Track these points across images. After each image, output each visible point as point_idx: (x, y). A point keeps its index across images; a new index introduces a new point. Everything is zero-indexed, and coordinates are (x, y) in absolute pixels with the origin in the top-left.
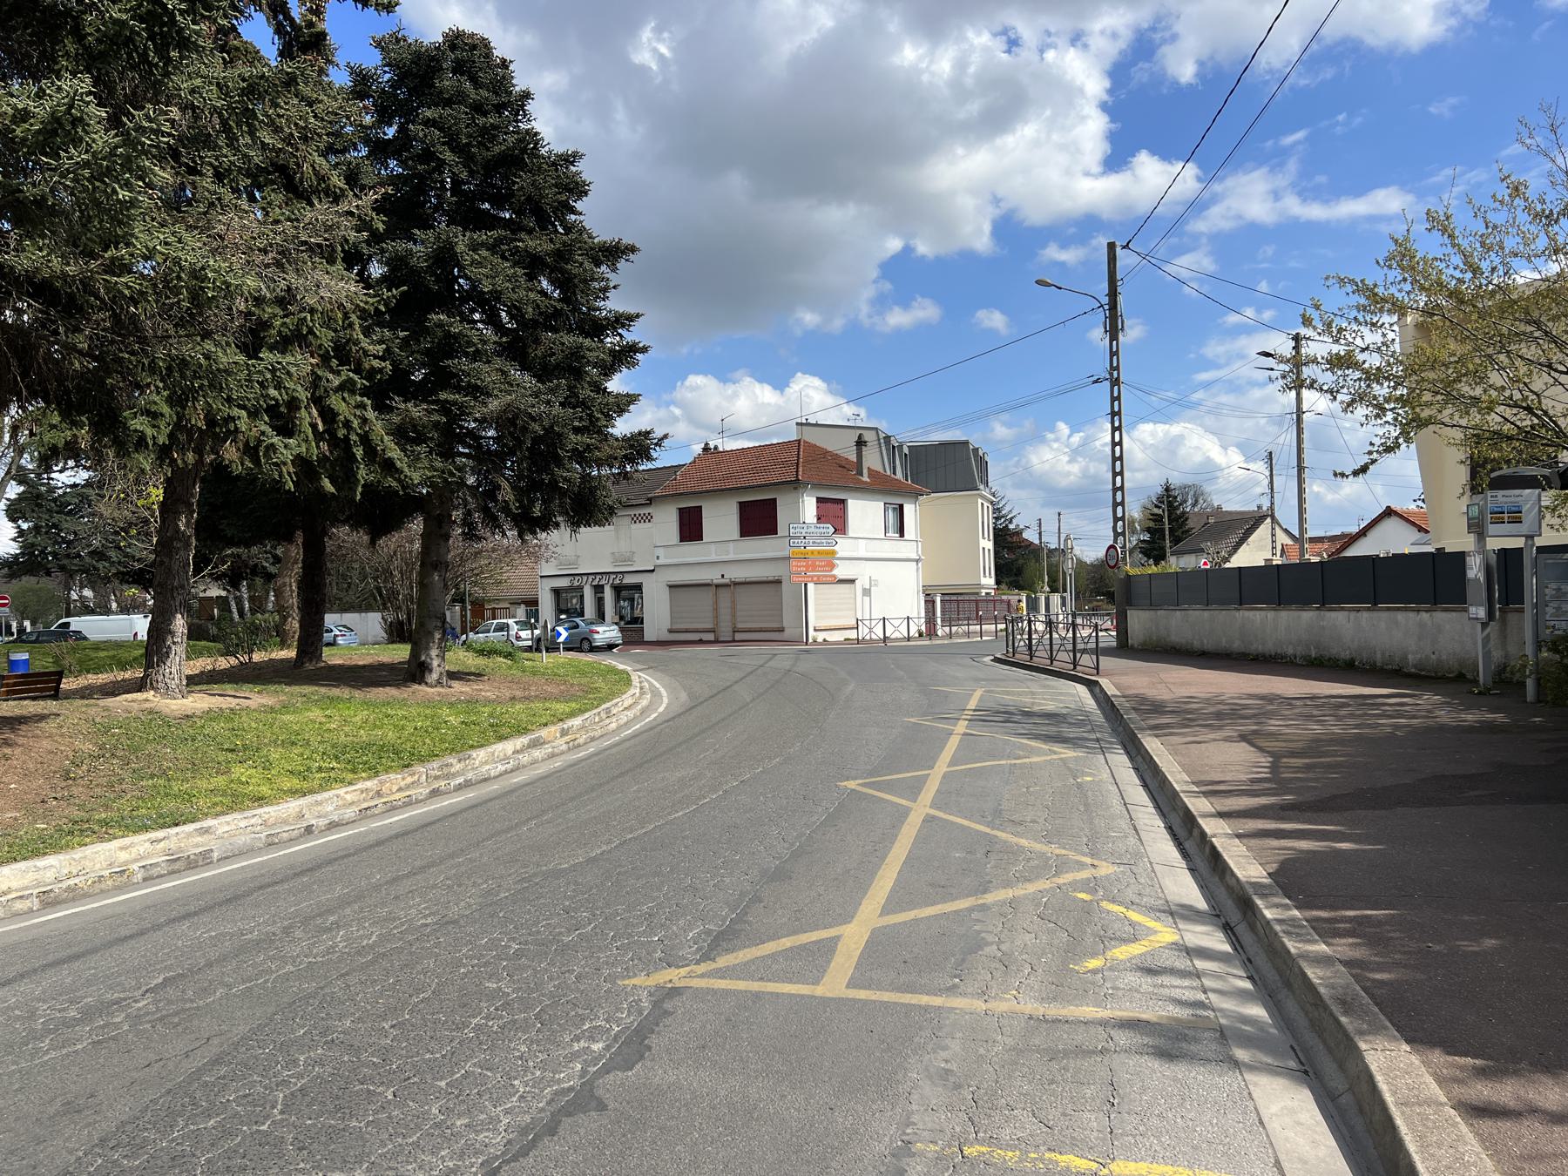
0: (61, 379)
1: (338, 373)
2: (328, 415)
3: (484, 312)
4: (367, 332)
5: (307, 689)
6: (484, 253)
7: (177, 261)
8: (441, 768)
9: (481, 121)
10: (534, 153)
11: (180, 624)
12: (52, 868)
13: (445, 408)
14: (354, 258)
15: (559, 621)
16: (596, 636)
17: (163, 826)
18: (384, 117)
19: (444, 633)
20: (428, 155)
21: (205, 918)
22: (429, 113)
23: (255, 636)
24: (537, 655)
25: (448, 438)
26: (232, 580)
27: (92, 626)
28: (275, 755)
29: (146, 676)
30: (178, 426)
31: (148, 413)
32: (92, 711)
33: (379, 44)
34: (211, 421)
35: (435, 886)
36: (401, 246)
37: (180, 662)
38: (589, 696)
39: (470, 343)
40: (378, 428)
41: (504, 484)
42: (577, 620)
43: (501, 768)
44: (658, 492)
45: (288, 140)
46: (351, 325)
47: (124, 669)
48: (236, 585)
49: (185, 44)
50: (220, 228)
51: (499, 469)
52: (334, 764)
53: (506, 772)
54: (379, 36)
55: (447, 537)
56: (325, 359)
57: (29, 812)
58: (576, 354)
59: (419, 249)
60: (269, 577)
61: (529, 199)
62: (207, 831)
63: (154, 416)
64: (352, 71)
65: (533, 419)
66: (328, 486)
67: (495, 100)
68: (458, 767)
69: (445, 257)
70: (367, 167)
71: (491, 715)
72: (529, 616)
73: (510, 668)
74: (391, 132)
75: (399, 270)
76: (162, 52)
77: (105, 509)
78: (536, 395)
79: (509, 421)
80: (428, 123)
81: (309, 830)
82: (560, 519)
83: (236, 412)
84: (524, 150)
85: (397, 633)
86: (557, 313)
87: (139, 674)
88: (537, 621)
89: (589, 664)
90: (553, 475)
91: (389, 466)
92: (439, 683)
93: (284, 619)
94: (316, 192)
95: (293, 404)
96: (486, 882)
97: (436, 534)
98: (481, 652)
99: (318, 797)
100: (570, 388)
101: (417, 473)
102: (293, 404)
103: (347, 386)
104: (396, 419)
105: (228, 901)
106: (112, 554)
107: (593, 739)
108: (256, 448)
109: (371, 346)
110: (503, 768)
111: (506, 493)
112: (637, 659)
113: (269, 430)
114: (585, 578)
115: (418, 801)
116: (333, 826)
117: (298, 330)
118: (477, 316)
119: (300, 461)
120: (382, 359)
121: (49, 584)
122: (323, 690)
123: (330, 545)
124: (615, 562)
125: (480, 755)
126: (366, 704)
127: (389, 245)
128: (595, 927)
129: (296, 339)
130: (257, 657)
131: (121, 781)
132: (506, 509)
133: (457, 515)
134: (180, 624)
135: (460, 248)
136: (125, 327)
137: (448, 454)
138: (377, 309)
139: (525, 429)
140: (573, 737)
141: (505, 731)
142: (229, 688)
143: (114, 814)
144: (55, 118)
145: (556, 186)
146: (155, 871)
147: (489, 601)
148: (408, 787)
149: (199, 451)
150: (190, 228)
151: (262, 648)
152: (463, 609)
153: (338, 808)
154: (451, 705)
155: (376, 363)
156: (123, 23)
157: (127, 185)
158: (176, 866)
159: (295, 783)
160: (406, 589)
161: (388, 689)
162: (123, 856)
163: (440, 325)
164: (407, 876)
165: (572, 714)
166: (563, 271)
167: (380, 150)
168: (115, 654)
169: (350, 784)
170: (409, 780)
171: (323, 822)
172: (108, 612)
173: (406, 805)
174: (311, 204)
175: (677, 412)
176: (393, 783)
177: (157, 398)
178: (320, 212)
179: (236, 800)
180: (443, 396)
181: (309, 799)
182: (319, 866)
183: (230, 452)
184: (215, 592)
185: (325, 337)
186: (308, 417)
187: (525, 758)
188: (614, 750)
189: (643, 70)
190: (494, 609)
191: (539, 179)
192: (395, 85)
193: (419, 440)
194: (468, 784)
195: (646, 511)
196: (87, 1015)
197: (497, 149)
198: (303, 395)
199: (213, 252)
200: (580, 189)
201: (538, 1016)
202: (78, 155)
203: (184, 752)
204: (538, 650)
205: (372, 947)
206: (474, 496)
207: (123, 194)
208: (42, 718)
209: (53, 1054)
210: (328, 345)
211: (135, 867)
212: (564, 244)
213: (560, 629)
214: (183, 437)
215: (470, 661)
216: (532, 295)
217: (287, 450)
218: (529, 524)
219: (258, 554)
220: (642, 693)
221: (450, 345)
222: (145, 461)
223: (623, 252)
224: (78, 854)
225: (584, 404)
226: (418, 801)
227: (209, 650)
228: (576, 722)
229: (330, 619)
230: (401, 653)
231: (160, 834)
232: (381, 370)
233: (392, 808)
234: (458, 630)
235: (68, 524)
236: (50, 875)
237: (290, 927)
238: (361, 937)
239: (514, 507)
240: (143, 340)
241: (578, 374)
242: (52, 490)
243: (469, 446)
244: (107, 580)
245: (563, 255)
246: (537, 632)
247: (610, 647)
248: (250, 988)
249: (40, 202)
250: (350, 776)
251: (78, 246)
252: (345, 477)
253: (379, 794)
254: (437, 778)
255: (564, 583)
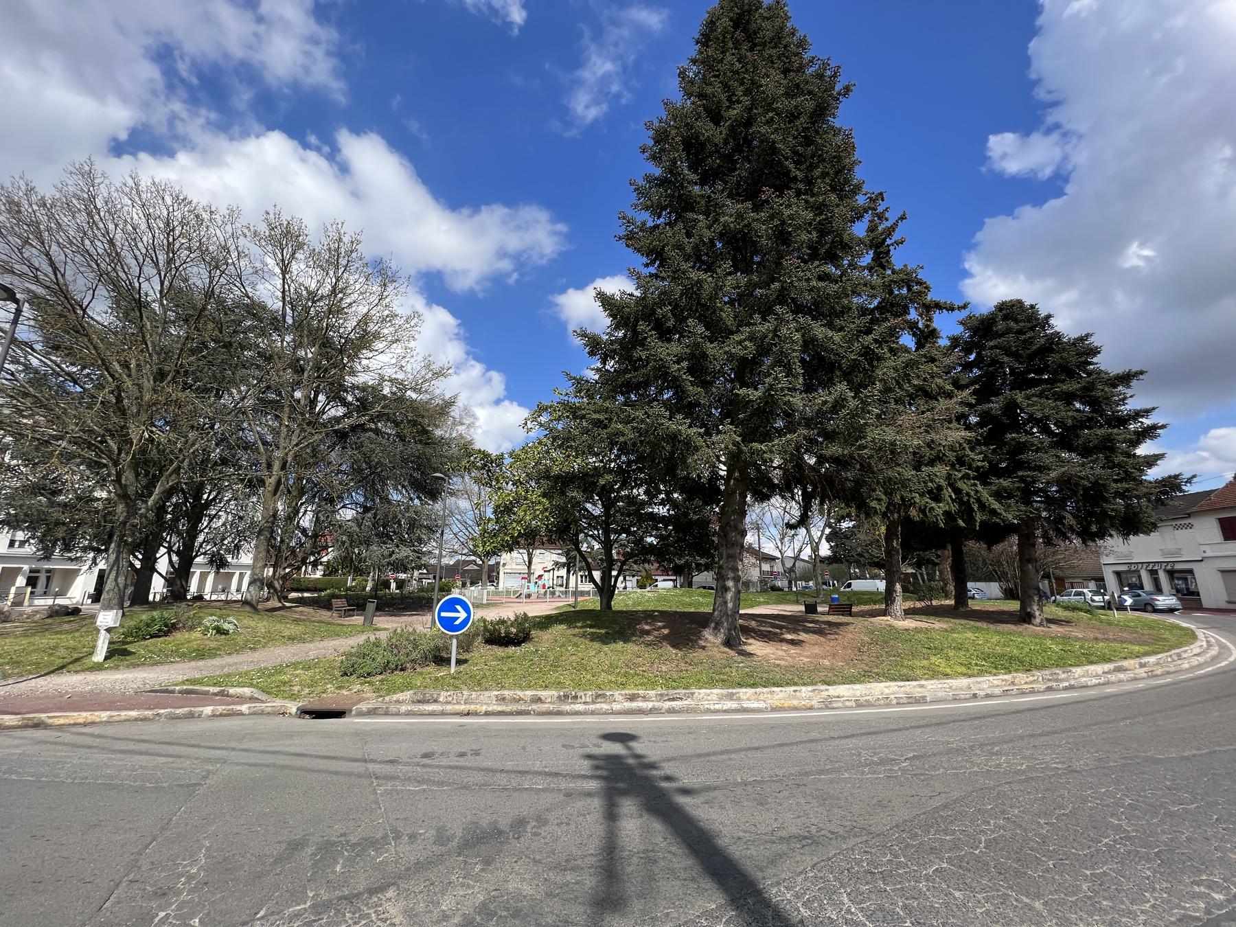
0: (844, 490)
1: (960, 471)
2: (958, 491)
3: (1039, 427)
4: (972, 449)
5: (963, 622)
6: (1035, 399)
7: (884, 440)
8: (1051, 674)
9: (1022, 337)
10: (1060, 342)
11: (898, 587)
12: (858, 690)
13: (1022, 480)
14: (961, 418)
15: (1123, 592)
16: (1157, 603)
17: (902, 680)
18: (968, 351)
19: (1040, 597)
20: (994, 362)
21: (927, 730)
22: (992, 344)
23: (931, 593)
24: (1109, 612)
25: (1026, 496)
26: (918, 565)
27: (858, 585)
28: (951, 654)
29: (886, 610)
30: (889, 504)
31: (877, 499)
32: (866, 623)
33: (961, 323)
34: (903, 499)
35: (1060, 746)
36: (986, 406)
37: (900, 605)
38: (1158, 643)
39: (1033, 445)
40: (985, 494)
41: (1068, 515)
42: (1139, 592)
43: (1095, 681)
44: (1195, 509)
45: (925, 380)
46: (964, 449)
47: (875, 604)
48: (920, 569)
49: (879, 359)
50: (900, 422)
51: (1063, 507)
52: (983, 663)
53: (1099, 684)
54: (960, 319)
55: (1033, 545)
56: (953, 466)
57: (848, 664)
58: (1109, 439)
59: (995, 405)
60: (935, 564)
61: (1060, 366)
62: (922, 686)
63: (879, 500)
64: (949, 338)
65: (1082, 478)
66: (961, 523)
67: (1029, 325)
68: (1063, 676)
69: (1011, 407)
70: (962, 376)
71: (1081, 647)
72: (1099, 587)
73: (1090, 619)
74: (972, 357)
75: (986, 418)
76: (871, 364)
77: (861, 536)
78: (1083, 465)
79: (1066, 483)
80: (992, 348)
81: (975, 696)
82: (1113, 533)
83: (914, 495)
84: (1052, 343)
85: (1010, 594)
86: (1090, 419)
87: (883, 606)
88: (1105, 590)
89: (1154, 621)
90: (1102, 507)
91: (993, 512)
92: (1041, 625)
93: (946, 585)
94: (939, 394)
95: (940, 488)
96: (1097, 752)
97: (1027, 542)
98: (1067, 608)
99: (979, 679)
100: (1106, 458)
101: (1011, 514)
102: (940, 488)
103: (966, 477)
104: (994, 488)
105: (938, 724)
106: (866, 555)
107: (1168, 673)
108: (925, 509)
109: (976, 458)
110: (1097, 682)
111: (1070, 520)
112: (1197, 620)
113: (930, 501)
114: (1140, 566)
115: (1039, 692)
116: (988, 696)
117: (938, 455)
118: (1035, 430)
119: (947, 513)
120: (983, 461)
121: (843, 567)
122: (972, 623)
123: (965, 549)
124: (1164, 554)
125: (1078, 671)
126: (998, 633)
127: (979, 408)
128: (1198, 807)
129: (937, 459)
130: (934, 603)
131: (882, 656)
132: (1072, 529)
133: (1038, 532)
134: (898, 587)
135: (1020, 400)
136: (866, 468)
137: (1027, 502)
138: (976, 439)
139: (1077, 485)
140: (1151, 669)
141: (1093, 658)
142: (923, 618)
143: (880, 670)
144: (836, 401)
145: (1077, 354)
146: (902, 701)
147: (1067, 578)
148: (1031, 682)
149: (899, 512)
150: (888, 426)
151: (937, 598)
152: (1050, 582)
153: (989, 687)
154: (1052, 639)
155: (980, 464)
156: (855, 360)
157: (863, 418)
158: (910, 700)
159: (964, 670)
160: (1013, 571)
161: (1009, 626)
162: (887, 691)
163: (1013, 439)
164: (1039, 735)
165: (1147, 654)
166: (1089, 397)
167: (968, 366)
168: (869, 597)
169: (995, 675)
170: (1031, 679)
171: (982, 693)
172: (866, 579)
173: (1031, 692)
174: (937, 400)
175: (1205, 454)
176: (1022, 678)
177: (879, 493)
178: (943, 403)
179: (934, 674)
180: (1020, 473)
181: (972, 680)
182: (984, 717)
183: (913, 513)
184: (910, 571)
185: (951, 456)
186: (948, 493)
187: (1113, 678)
188: (1190, 683)
189: (1134, 269)
190: (1072, 583)
191: (1065, 355)
192: (971, 337)
193: (1009, 497)
194: (1071, 688)
195: (1187, 521)
196: (882, 762)
197: (1034, 348)
198: (944, 483)
199: (898, 433)
200: (1095, 351)
201: (1157, 854)
202: (845, 412)
203: (907, 646)
204: (1110, 608)
205: (1024, 772)
206: (1048, 523)
207: (862, 422)
208: (848, 624)
209: (870, 776)
210: (953, 459)
211: (892, 697)
212: (1088, 382)
213: (1125, 597)
214: (892, 508)
215: (1061, 613)
216: (1070, 414)
217: (939, 509)
218: (1088, 536)
219: (930, 555)
220: (1209, 645)
221: (1021, 448)
222: (877, 519)
223: (1134, 376)
224: (869, 686)
225: (1119, 466)
226: (1039, 692)
227: (911, 598)
228: (1152, 659)
229: (970, 585)
230: (1014, 606)
231: (902, 683)
232: (982, 467)
233: (1022, 693)
234: (1049, 594)
235: (848, 543)
236: (858, 693)
237: (972, 746)
238: (1016, 764)
239: (1077, 528)
240: (873, 473)
241: (1112, 449)
242: (841, 529)
243: (1041, 497)
244: (864, 565)
245: (1090, 387)
246: (1107, 598)
247: (1171, 611)
248: (957, 774)
249: (834, 431)
250: (994, 671)
251: (846, 442)
252: (970, 519)
253: (1013, 683)
254: (1049, 680)
255: (1124, 568)
